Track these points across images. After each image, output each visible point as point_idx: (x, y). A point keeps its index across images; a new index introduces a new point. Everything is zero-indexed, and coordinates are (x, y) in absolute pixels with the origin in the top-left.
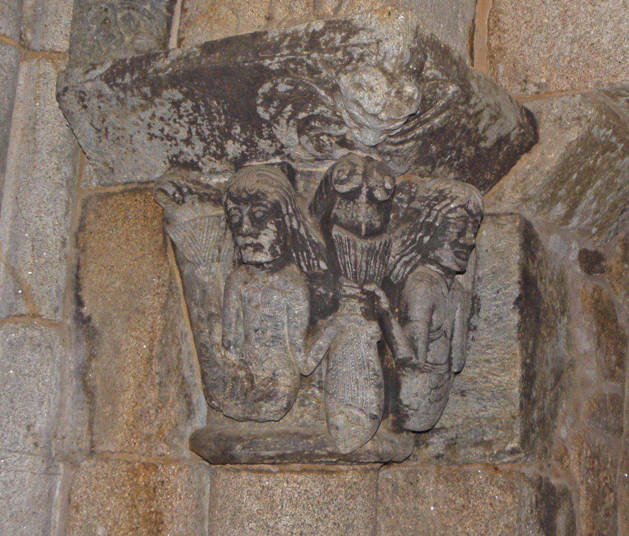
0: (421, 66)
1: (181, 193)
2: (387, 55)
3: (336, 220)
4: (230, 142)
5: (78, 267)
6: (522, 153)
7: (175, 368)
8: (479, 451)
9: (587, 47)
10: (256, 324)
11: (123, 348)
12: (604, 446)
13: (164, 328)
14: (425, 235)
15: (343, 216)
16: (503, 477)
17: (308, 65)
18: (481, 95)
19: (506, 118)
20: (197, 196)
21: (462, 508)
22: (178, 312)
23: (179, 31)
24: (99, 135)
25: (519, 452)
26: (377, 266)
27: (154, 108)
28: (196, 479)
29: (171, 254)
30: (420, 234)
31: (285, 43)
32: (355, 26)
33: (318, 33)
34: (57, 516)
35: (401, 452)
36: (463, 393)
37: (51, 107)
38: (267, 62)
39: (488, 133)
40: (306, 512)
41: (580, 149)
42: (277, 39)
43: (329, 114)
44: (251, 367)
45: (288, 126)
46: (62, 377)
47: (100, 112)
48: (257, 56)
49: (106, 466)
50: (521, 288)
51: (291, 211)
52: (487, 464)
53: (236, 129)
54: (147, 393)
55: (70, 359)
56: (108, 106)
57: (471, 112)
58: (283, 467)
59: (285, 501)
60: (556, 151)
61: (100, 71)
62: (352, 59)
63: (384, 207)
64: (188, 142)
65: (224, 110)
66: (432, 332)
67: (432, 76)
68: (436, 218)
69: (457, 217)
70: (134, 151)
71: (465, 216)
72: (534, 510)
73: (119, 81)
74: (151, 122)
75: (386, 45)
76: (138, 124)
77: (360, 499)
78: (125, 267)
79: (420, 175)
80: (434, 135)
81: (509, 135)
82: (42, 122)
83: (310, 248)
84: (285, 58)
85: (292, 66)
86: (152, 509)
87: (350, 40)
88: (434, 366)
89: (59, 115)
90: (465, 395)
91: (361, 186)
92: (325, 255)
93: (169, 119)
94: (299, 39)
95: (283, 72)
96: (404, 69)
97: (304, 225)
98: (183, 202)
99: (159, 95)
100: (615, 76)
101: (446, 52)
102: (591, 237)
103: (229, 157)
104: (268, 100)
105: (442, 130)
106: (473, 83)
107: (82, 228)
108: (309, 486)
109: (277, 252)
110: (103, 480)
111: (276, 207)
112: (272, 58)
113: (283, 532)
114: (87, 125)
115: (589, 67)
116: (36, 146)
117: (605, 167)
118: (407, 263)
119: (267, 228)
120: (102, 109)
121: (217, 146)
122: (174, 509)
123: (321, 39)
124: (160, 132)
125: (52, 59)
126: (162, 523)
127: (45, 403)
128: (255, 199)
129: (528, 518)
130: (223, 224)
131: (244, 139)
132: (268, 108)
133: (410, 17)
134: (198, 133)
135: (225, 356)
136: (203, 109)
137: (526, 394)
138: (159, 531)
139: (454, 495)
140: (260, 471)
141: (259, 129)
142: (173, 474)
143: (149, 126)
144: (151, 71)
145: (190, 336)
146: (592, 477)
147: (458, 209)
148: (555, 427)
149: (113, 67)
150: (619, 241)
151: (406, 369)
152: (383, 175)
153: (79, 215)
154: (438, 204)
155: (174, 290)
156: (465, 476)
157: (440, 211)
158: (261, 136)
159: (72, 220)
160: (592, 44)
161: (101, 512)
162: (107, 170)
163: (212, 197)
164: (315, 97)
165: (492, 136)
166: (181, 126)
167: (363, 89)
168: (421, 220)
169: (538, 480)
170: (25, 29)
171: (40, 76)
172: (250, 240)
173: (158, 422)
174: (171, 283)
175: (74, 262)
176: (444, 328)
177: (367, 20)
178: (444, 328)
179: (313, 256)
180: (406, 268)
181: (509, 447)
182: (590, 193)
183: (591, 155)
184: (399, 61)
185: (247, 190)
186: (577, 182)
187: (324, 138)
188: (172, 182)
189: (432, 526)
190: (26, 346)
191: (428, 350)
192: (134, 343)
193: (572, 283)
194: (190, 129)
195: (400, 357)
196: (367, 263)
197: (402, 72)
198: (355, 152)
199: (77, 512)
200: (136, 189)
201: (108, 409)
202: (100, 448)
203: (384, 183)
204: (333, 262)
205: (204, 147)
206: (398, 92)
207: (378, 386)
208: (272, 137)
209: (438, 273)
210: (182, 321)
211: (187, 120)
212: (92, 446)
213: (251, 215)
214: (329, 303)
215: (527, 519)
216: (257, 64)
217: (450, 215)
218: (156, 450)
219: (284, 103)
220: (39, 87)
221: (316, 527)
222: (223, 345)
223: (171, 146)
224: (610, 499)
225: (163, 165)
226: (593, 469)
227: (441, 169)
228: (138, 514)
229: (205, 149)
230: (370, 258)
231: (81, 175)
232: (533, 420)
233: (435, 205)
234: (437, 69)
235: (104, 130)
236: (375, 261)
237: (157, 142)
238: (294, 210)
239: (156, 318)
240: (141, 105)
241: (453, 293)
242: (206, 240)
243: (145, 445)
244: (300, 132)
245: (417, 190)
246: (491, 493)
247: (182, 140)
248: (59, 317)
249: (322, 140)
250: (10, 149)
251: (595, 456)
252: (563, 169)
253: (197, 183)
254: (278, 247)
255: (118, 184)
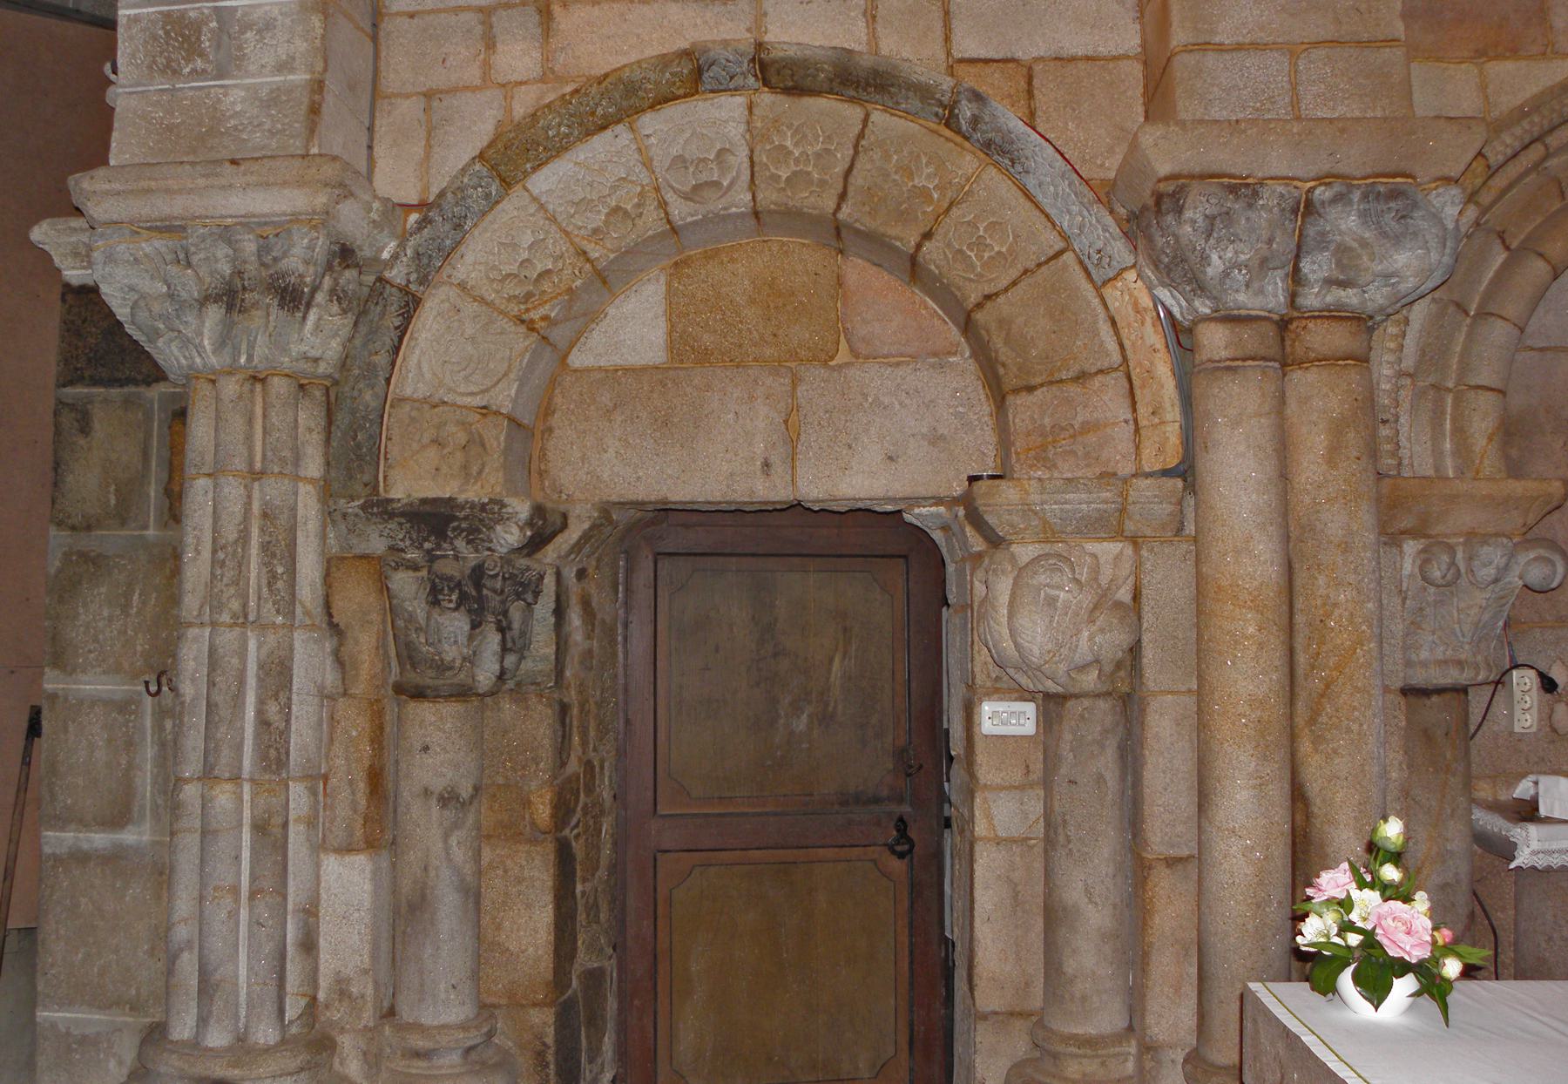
3: (484, 586)
8: (533, 687)
61: (357, 503)
95: (466, 518)
96: (526, 524)
156: (526, 700)
208: (451, 543)
219: (462, 531)
244: (468, 543)
251: (581, 685)
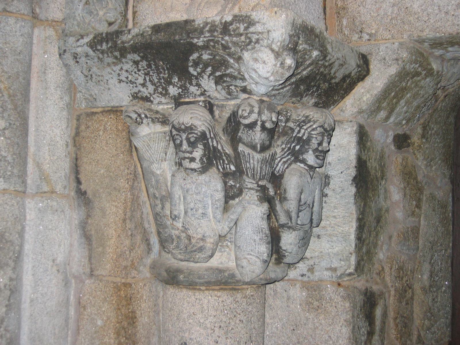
0: (296, 44)
1: (141, 118)
2: (275, 40)
3: (240, 140)
4: (171, 87)
5: (77, 159)
6: (358, 81)
7: (139, 224)
9: (403, 10)
10: (192, 205)
11: (108, 212)
12: (406, 261)
13: (132, 201)
14: (297, 145)
15: (245, 138)
16: (344, 290)
17: (222, 44)
18: (333, 54)
19: (349, 64)
20: (151, 119)
21: (317, 308)
22: (140, 189)
23: (133, 6)
24: (87, 79)
25: (354, 275)
26: (267, 169)
27: (122, 65)
28: (154, 289)
29: (134, 154)
30: (293, 145)
31: (207, 29)
32: (253, 20)
33: (228, 23)
34: (72, 312)
35: (280, 276)
36: (319, 237)
37: (54, 60)
38: (195, 40)
39: (337, 75)
40: (223, 314)
41: (397, 79)
42: (201, 25)
43: (236, 74)
44: (189, 231)
45: (209, 80)
46: (71, 228)
47: (87, 65)
48: (188, 36)
49: (101, 284)
50: (357, 171)
51: (212, 136)
52: (333, 281)
53: (175, 79)
54: (124, 241)
55: (75, 217)
56: (92, 62)
57: (327, 64)
58: (208, 288)
59: (210, 308)
60: (381, 81)
61: (86, 40)
62: (251, 42)
63: (271, 133)
64: (143, 85)
65: (167, 68)
66: (301, 206)
67: (303, 49)
68: (304, 134)
69: (318, 134)
70: (109, 89)
71: (323, 132)
72: (362, 309)
73: (99, 48)
74: (120, 72)
75: (274, 34)
76: (112, 74)
77: (255, 304)
78: (106, 160)
79: (293, 103)
80: (302, 80)
81: (351, 73)
82: (50, 68)
83: (224, 158)
84: (207, 39)
85: (212, 44)
86: (130, 310)
87: (250, 29)
88: (302, 226)
89: (60, 63)
90: (320, 238)
91: (257, 121)
92: (234, 161)
93: (132, 71)
94: (217, 26)
95: (206, 47)
97: (220, 143)
98: (142, 123)
99: (125, 57)
100: (422, 31)
101: (312, 31)
102: (402, 126)
103: (170, 95)
104: (196, 64)
105: (307, 77)
106: (329, 47)
107: (77, 134)
108: (224, 298)
109: (204, 161)
110: (99, 292)
111: (203, 134)
112: (198, 38)
113: (209, 326)
114: (79, 73)
115: (404, 24)
116: (47, 84)
117: (413, 86)
118: (285, 162)
119: (198, 147)
120: (89, 64)
121: (163, 89)
122: (142, 309)
123: (230, 27)
124: (125, 79)
125: (53, 26)
126: (136, 318)
127: (62, 246)
128: (190, 129)
129: (358, 314)
130: (167, 138)
131: (180, 85)
132: (196, 69)
133: (289, 14)
134: (150, 81)
135: (173, 224)
136: (153, 67)
137: (359, 238)
138: (134, 323)
139: (312, 299)
140: (195, 289)
141: (189, 80)
142: (141, 288)
143: (119, 75)
144: (119, 42)
145: (148, 203)
146: (399, 281)
147: (318, 129)
148: (376, 253)
149: (95, 38)
150: (420, 125)
151: (285, 228)
152: (271, 113)
153: (75, 126)
154: (305, 125)
155: (138, 176)
157: (306, 129)
158: (191, 84)
159: (71, 129)
160: (407, 8)
161: (99, 311)
162: (92, 99)
163: (160, 120)
164: (227, 63)
165: (340, 75)
166: (139, 75)
167: (258, 62)
168: (294, 135)
169: (365, 290)
170: (35, 6)
171: (46, 38)
172: (187, 155)
173: (131, 259)
174: (135, 172)
175: (74, 155)
176: (308, 202)
177: (261, 17)
178: (308, 202)
179: (226, 162)
180: (284, 166)
181: (348, 271)
182: (402, 102)
183: (404, 80)
184: (282, 44)
185: (185, 123)
186: (394, 97)
187: (233, 88)
188: (135, 111)
189: (298, 318)
190: (49, 212)
191: (298, 217)
192: (114, 209)
193: (389, 156)
194: (145, 77)
195: (281, 223)
196: (261, 168)
197: (284, 50)
198: (252, 96)
199: (85, 309)
200: (111, 110)
201: (100, 249)
202: (96, 273)
203: (271, 118)
204: (238, 166)
205: (154, 89)
206: (282, 64)
207: (268, 243)
208: (199, 85)
209: (305, 169)
210: (143, 194)
211: (143, 72)
212: (92, 271)
213: (188, 139)
214: (237, 190)
215: (358, 315)
216: (189, 42)
217: (313, 133)
218: (131, 275)
219: (206, 66)
220: (46, 45)
221: (229, 323)
222: (171, 217)
223: (133, 87)
224: (409, 293)
225: (128, 97)
226: (399, 277)
227: (306, 98)
228: (122, 314)
229: (155, 90)
230: (263, 165)
231: (74, 100)
232: (363, 253)
233: (303, 126)
234: (306, 44)
235: (89, 76)
236: (266, 166)
237: (123, 84)
238: (214, 135)
239: (127, 194)
240: (114, 63)
241: (314, 180)
242: (158, 148)
243: (124, 272)
244: (217, 83)
245: (291, 114)
246: (335, 300)
247: (140, 84)
248: (67, 192)
249: (231, 89)
250: (31, 86)
252: (386, 91)
253: (150, 110)
254: (204, 158)
255: (98, 107)
